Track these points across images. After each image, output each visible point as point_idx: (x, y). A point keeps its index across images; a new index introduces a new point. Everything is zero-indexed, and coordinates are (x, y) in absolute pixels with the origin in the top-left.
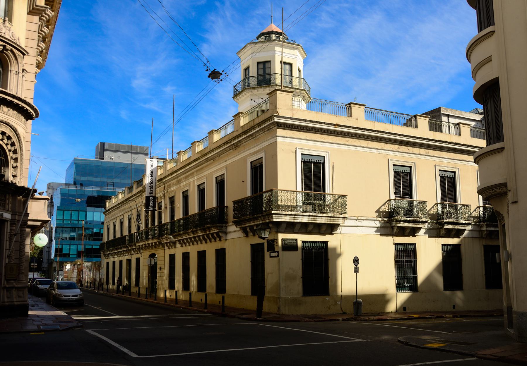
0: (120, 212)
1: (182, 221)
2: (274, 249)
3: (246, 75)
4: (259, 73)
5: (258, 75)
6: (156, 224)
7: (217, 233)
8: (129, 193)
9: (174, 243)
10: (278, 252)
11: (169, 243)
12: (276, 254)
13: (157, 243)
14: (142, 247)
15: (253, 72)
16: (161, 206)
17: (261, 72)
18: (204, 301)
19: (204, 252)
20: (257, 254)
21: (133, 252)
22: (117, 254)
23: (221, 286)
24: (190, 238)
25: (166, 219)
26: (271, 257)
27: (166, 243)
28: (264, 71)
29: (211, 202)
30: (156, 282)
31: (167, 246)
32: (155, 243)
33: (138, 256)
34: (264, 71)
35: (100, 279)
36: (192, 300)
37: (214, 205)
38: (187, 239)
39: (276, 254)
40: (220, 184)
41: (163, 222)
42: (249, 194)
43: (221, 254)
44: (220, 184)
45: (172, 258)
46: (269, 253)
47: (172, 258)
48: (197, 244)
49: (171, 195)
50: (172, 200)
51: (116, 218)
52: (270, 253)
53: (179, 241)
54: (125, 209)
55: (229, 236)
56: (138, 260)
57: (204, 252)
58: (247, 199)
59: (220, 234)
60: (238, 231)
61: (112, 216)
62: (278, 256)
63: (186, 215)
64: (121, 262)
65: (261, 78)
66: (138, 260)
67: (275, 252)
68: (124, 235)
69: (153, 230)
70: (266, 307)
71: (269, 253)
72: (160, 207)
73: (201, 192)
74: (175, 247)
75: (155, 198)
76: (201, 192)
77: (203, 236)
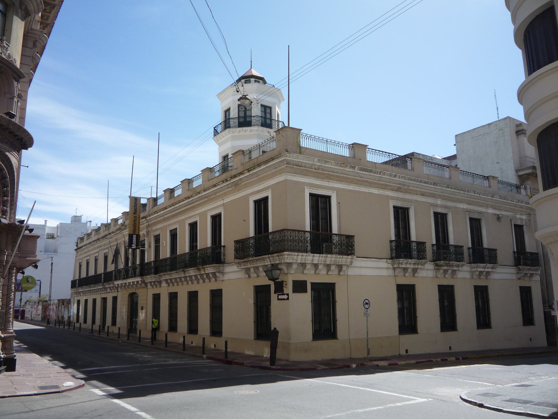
0: (95, 249)
1: (252, 241)
2: (282, 291)
3: (226, 117)
4: (240, 115)
5: (239, 117)
6: (130, 265)
7: (214, 274)
8: (106, 230)
9: (160, 282)
10: (288, 295)
11: (154, 282)
12: (286, 297)
13: (140, 282)
14: (121, 286)
15: (234, 113)
16: (144, 245)
17: (242, 114)
18: (91, 328)
19: (95, 299)
20: (262, 297)
21: (82, 294)
22: (90, 292)
23: (216, 329)
24: (180, 278)
25: (150, 257)
26: (278, 299)
27: (150, 282)
28: (245, 114)
29: (205, 240)
30: (136, 321)
31: (151, 285)
32: (138, 282)
33: (115, 294)
34: (245, 114)
35: (69, 317)
36: (168, 340)
37: (187, 250)
38: (176, 279)
39: (286, 297)
40: (216, 220)
41: (146, 261)
42: (252, 234)
43: (216, 296)
44: (216, 220)
45: (157, 298)
46: (276, 295)
47: (157, 298)
48: (198, 283)
49: (157, 233)
50: (157, 239)
51: (89, 255)
52: (278, 295)
53: (166, 280)
54: (100, 247)
55: (226, 277)
56: (115, 299)
57: (95, 299)
58: (207, 248)
59: (217, 274)
60: (238, 271)
61: (85, 253)
62: (288, 299)
63: (193, 250)
64: (94, 301)
65: (242, 120)
66: (115, 299)
67: (284, 294)
68: (99, 273)
69: (134, 269)
70: (279, 354)
71: (276, 295)
72: (143, 245)
73: (174, 235)
74: (160, 286)
75: (138, 236)
76: (174, 235)
77: (196, 276)
